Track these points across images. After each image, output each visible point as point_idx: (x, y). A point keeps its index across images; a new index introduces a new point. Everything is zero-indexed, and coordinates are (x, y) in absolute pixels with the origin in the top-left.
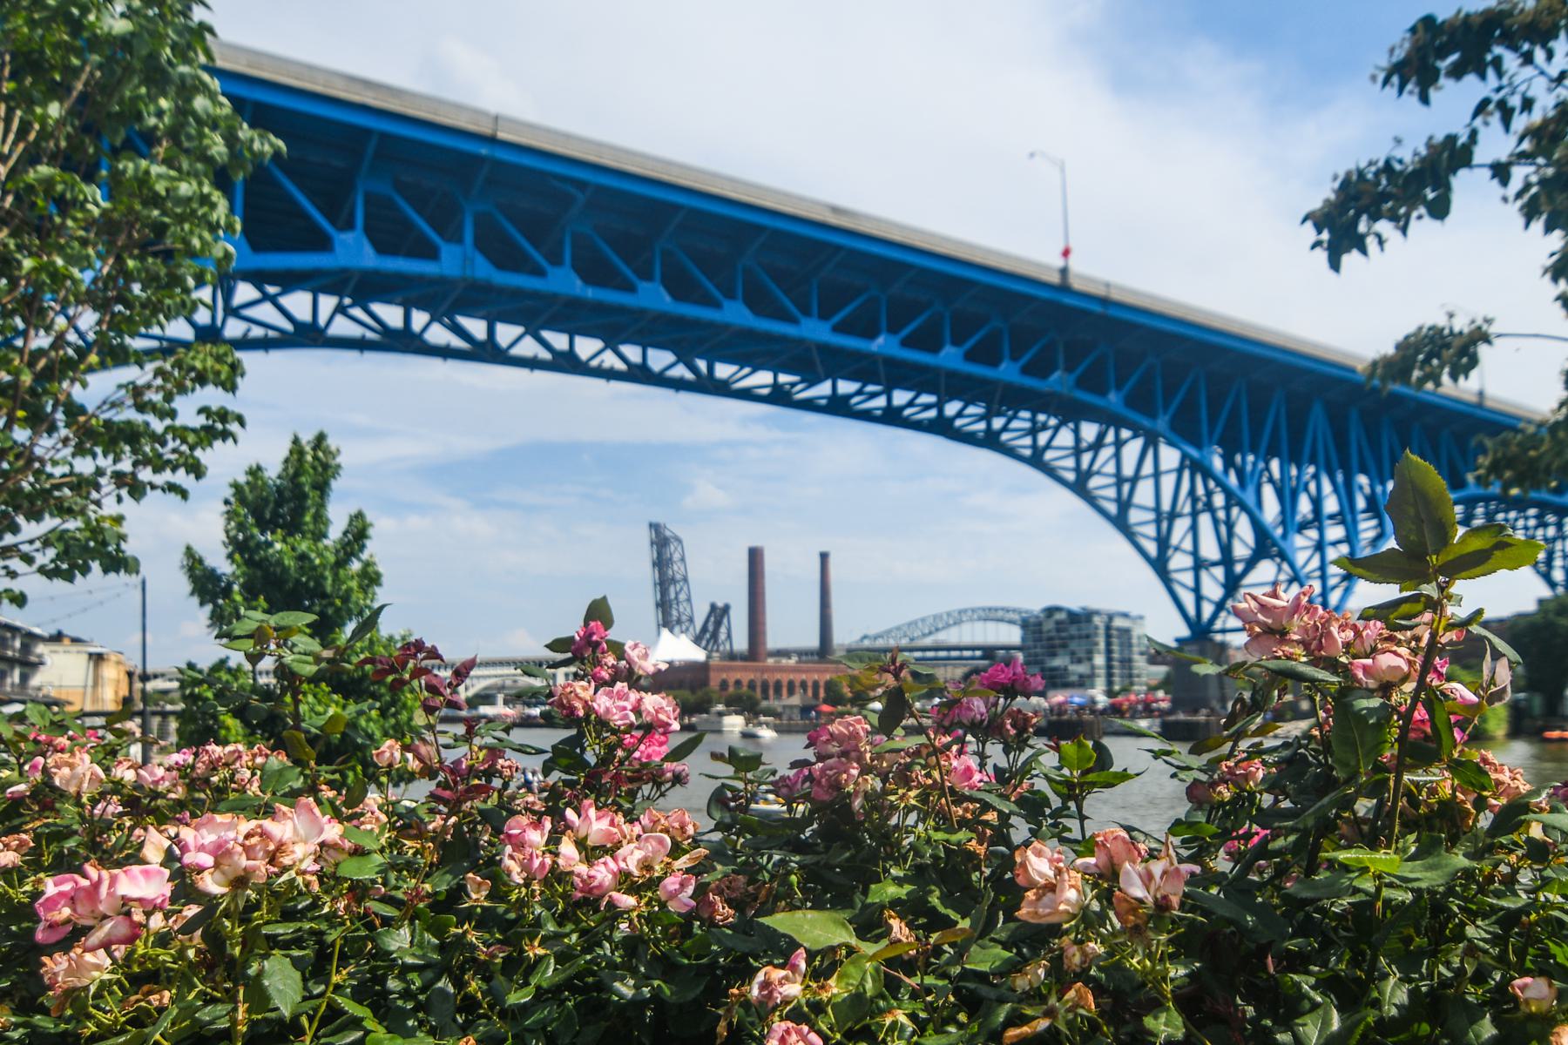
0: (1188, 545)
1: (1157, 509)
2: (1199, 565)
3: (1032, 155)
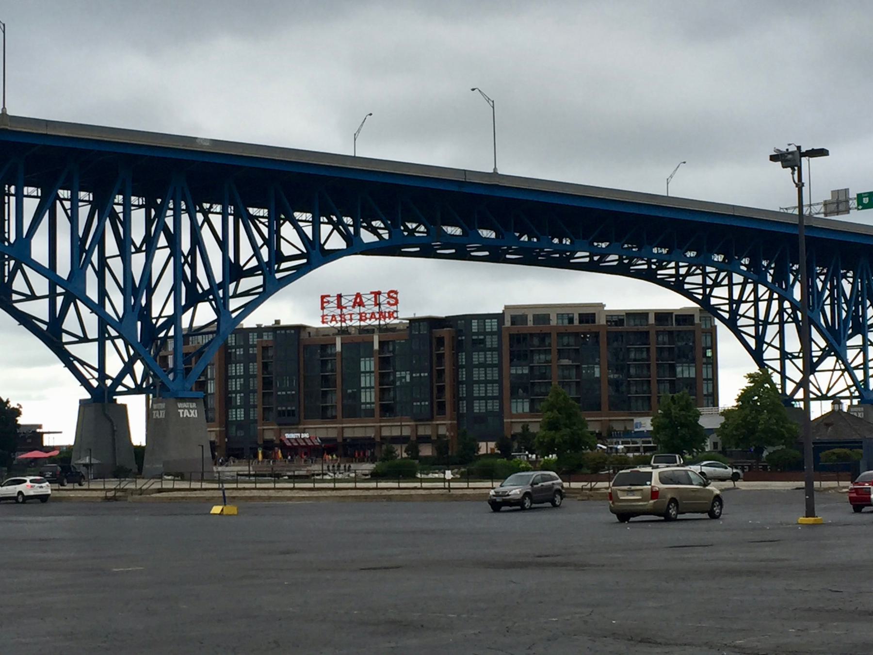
0: (776, 343)
1: (756, 318)
2: (784, 356)
3: (473, 90)
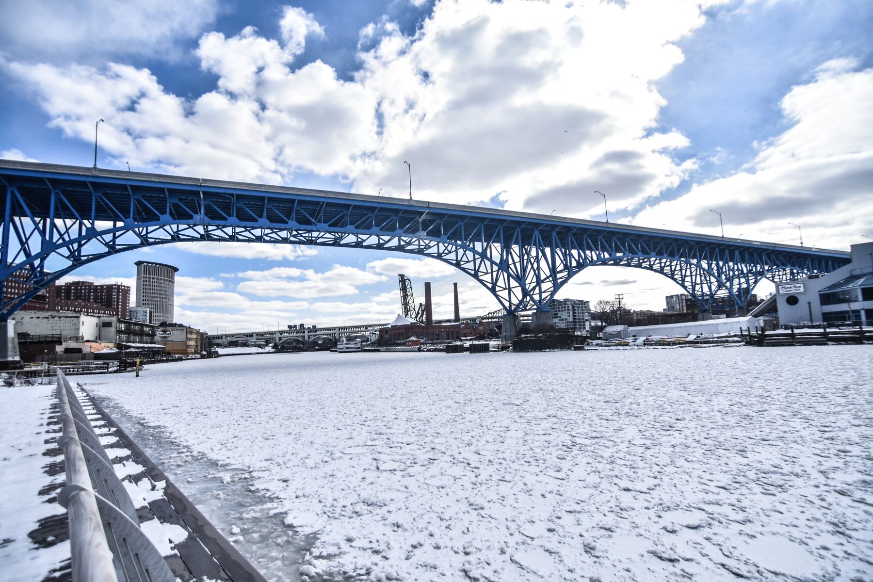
1: (692, 282)
